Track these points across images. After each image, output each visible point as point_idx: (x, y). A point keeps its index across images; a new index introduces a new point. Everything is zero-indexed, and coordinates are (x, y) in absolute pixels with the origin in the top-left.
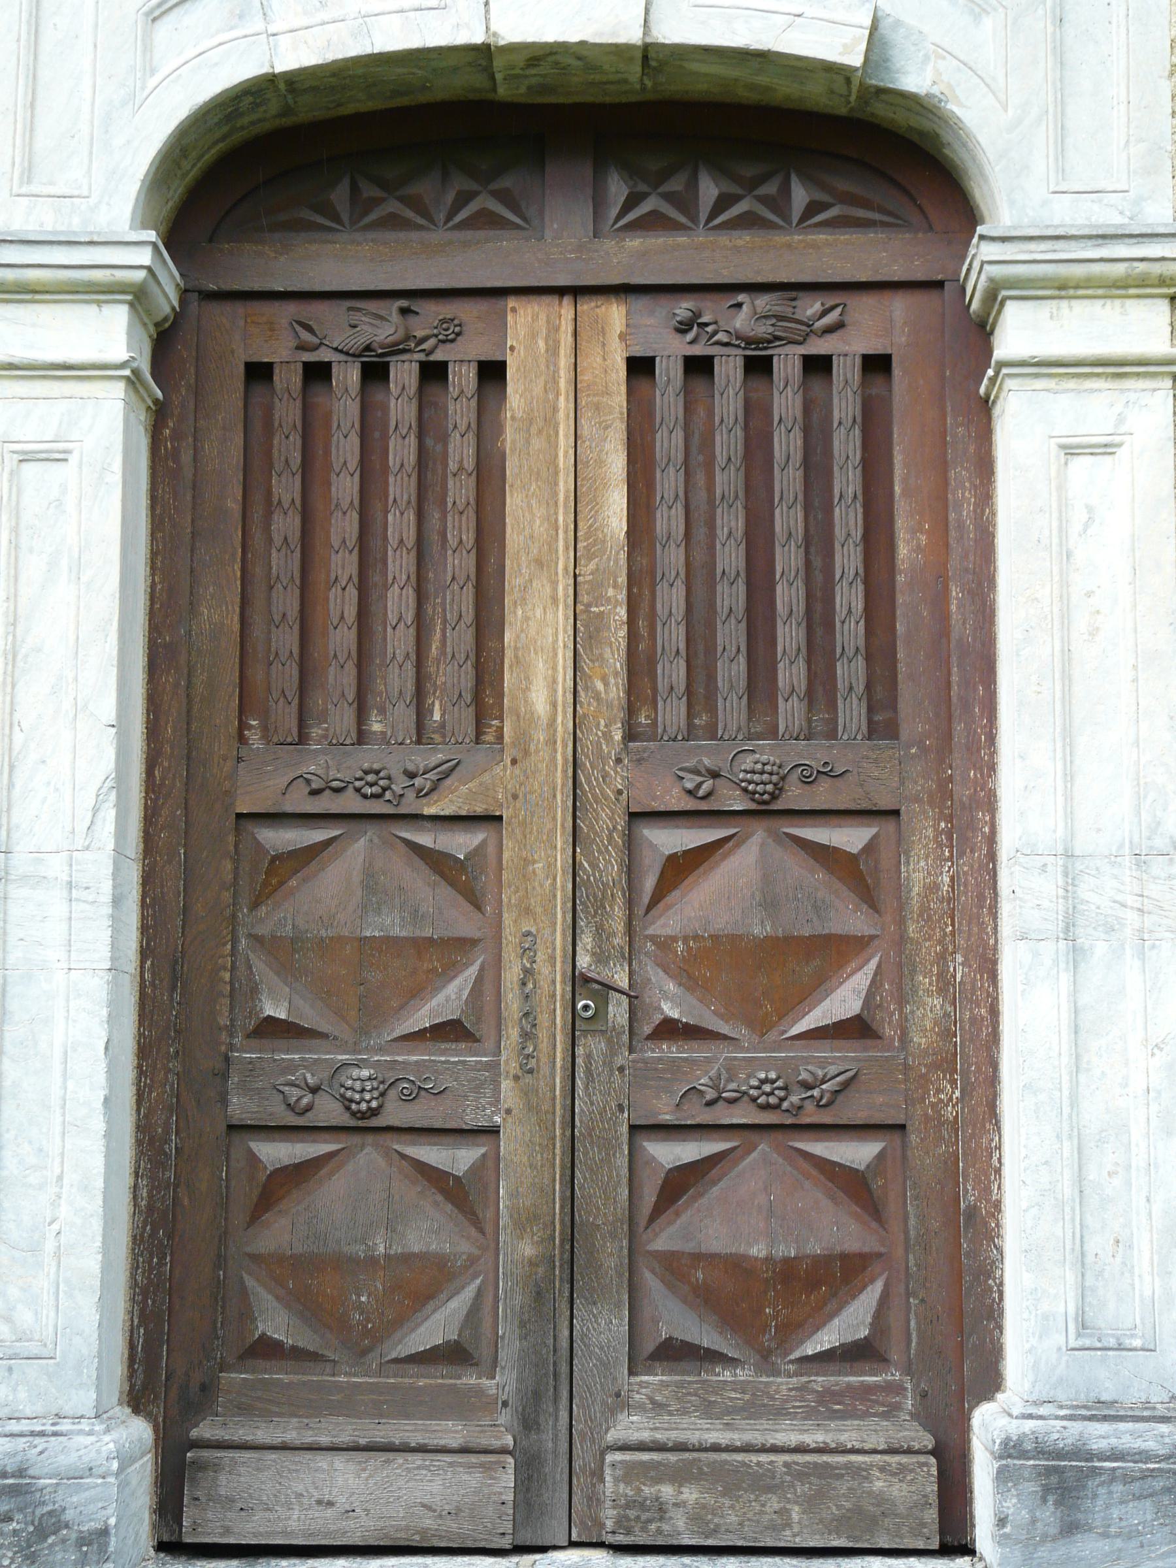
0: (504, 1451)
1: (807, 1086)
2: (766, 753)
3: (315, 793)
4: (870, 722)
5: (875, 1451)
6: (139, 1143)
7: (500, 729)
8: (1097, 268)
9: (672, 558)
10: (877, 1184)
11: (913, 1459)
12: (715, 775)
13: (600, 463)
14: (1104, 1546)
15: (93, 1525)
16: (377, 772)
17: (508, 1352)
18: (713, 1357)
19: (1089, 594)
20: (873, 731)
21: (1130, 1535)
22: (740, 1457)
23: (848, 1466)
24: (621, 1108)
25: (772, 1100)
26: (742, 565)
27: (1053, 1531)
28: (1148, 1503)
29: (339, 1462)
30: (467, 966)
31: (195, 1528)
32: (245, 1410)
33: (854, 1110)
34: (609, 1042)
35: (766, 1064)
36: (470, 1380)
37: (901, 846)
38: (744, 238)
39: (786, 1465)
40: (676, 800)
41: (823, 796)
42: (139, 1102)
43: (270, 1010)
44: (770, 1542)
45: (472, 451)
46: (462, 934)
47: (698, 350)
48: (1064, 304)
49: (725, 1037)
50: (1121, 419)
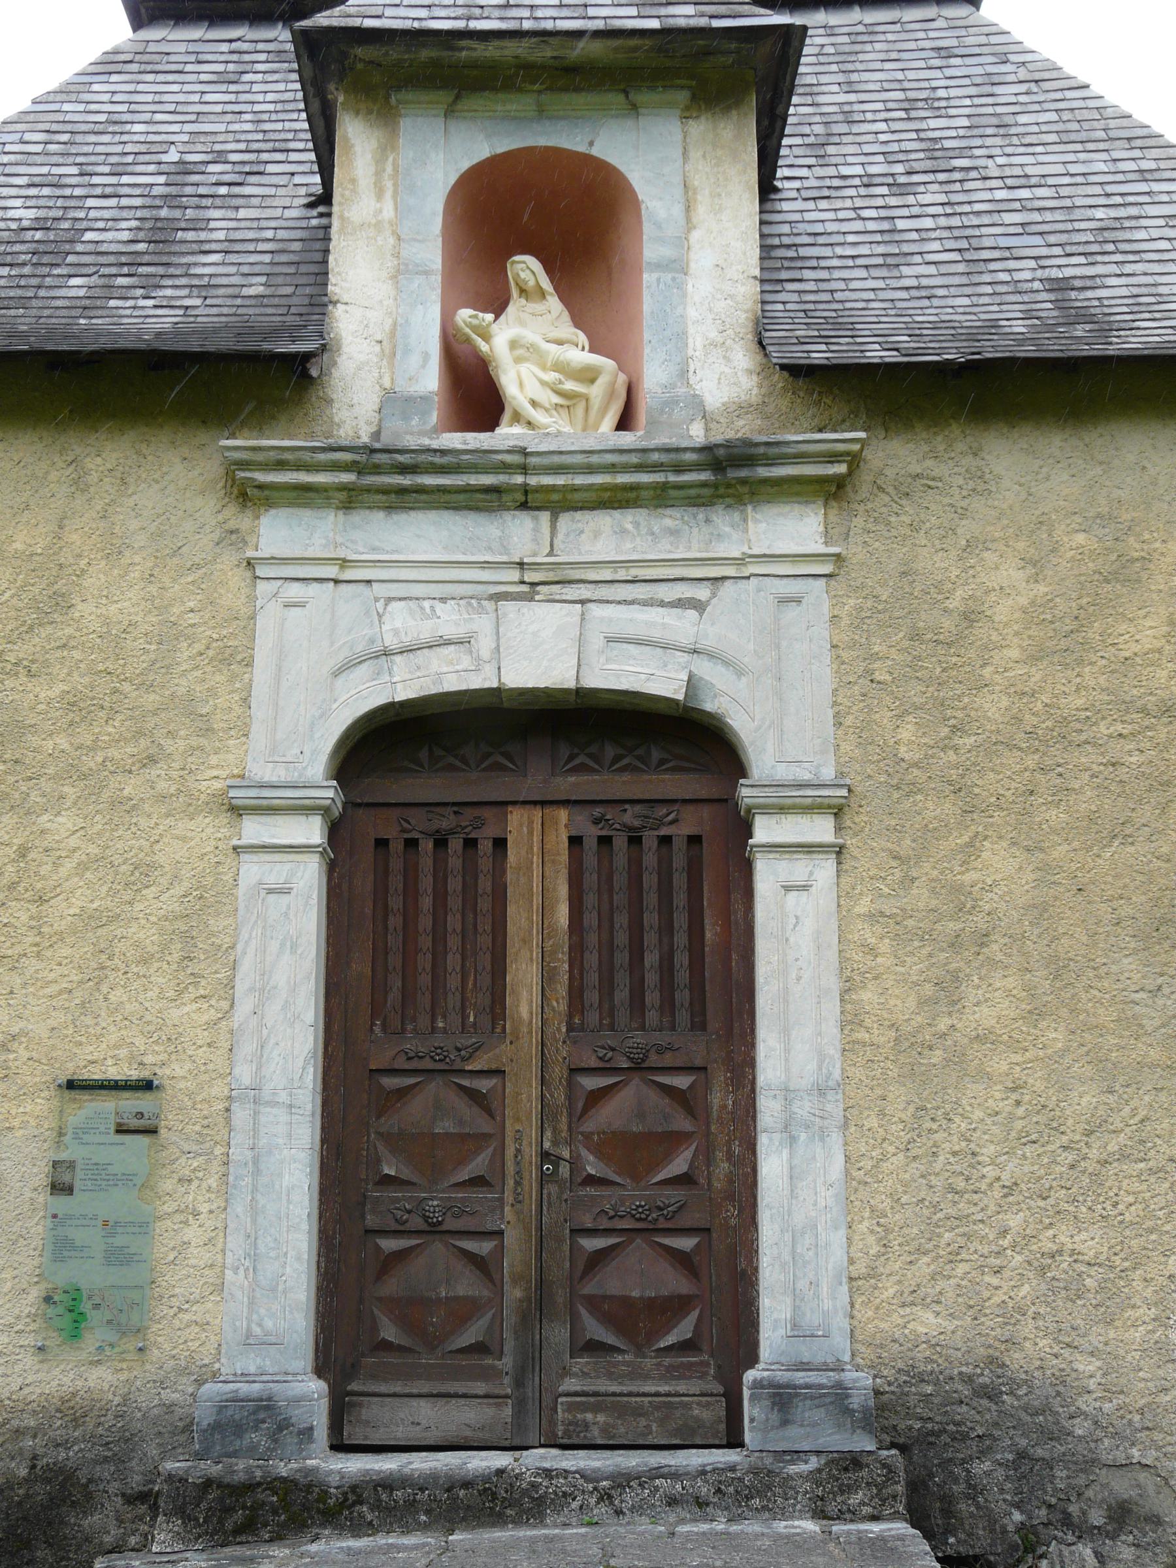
0: (507, 1397)
1: (660, 1209)
2: (639, 1038)
3: (409, 1059)
4: (692, 1021)
5: (694, 1395)
6: (320, 1239)
7: (504, 1027)
8: (798, 800)
9: (592, 939)
10: (696, 1259)
11: (714, 1399)
12: (613, 1049)
13: (555, 889)
14: (802, 1431)
15: (305, 1425)
16: (441, 1048)
17: (509, 1346)
18: (613, 1349)
19: (797, 960)
20: (693, 1028)
21: (814, 1425)
22: (625, 1399)
23: (680, 1403)
24: (566, 1221)
25: (643, 1216)
26: (627, 942)
27: (777, 1424)
28: (822, 1410)
29: (423, 1402)
30: (487, 1147)
31: (350, 1435)
32: (374, 1377)
33: (685, 1221)
34: (560, 1187)
35: (641, 1198)
36: (489, 1361)
37: (708, 1087)
38: (626, 777)
39: (650, 1402)
40: (593, 1063)
41: (668, 1060)
42: (320, 1218)
43: (386, 1171)
44: (641, 1442)
45: (489, 884)
46: (485, 1131)
47: (604, 833)
48: (783, 816)
49: (619, 1184)
50: (811, 873)
